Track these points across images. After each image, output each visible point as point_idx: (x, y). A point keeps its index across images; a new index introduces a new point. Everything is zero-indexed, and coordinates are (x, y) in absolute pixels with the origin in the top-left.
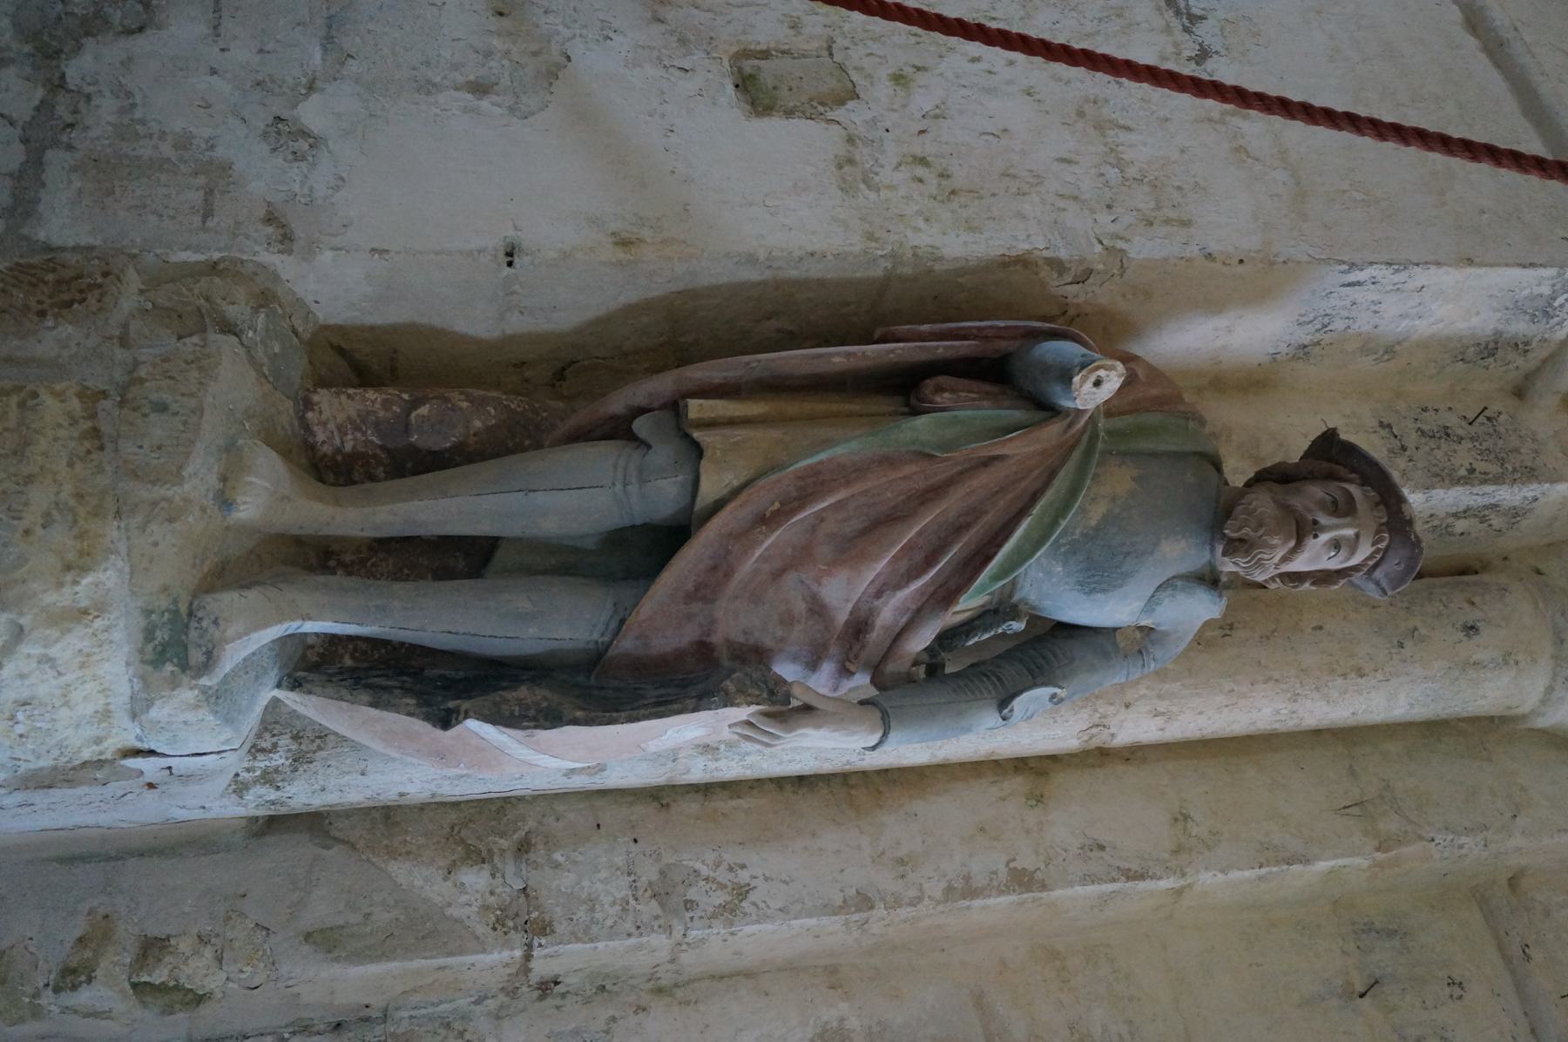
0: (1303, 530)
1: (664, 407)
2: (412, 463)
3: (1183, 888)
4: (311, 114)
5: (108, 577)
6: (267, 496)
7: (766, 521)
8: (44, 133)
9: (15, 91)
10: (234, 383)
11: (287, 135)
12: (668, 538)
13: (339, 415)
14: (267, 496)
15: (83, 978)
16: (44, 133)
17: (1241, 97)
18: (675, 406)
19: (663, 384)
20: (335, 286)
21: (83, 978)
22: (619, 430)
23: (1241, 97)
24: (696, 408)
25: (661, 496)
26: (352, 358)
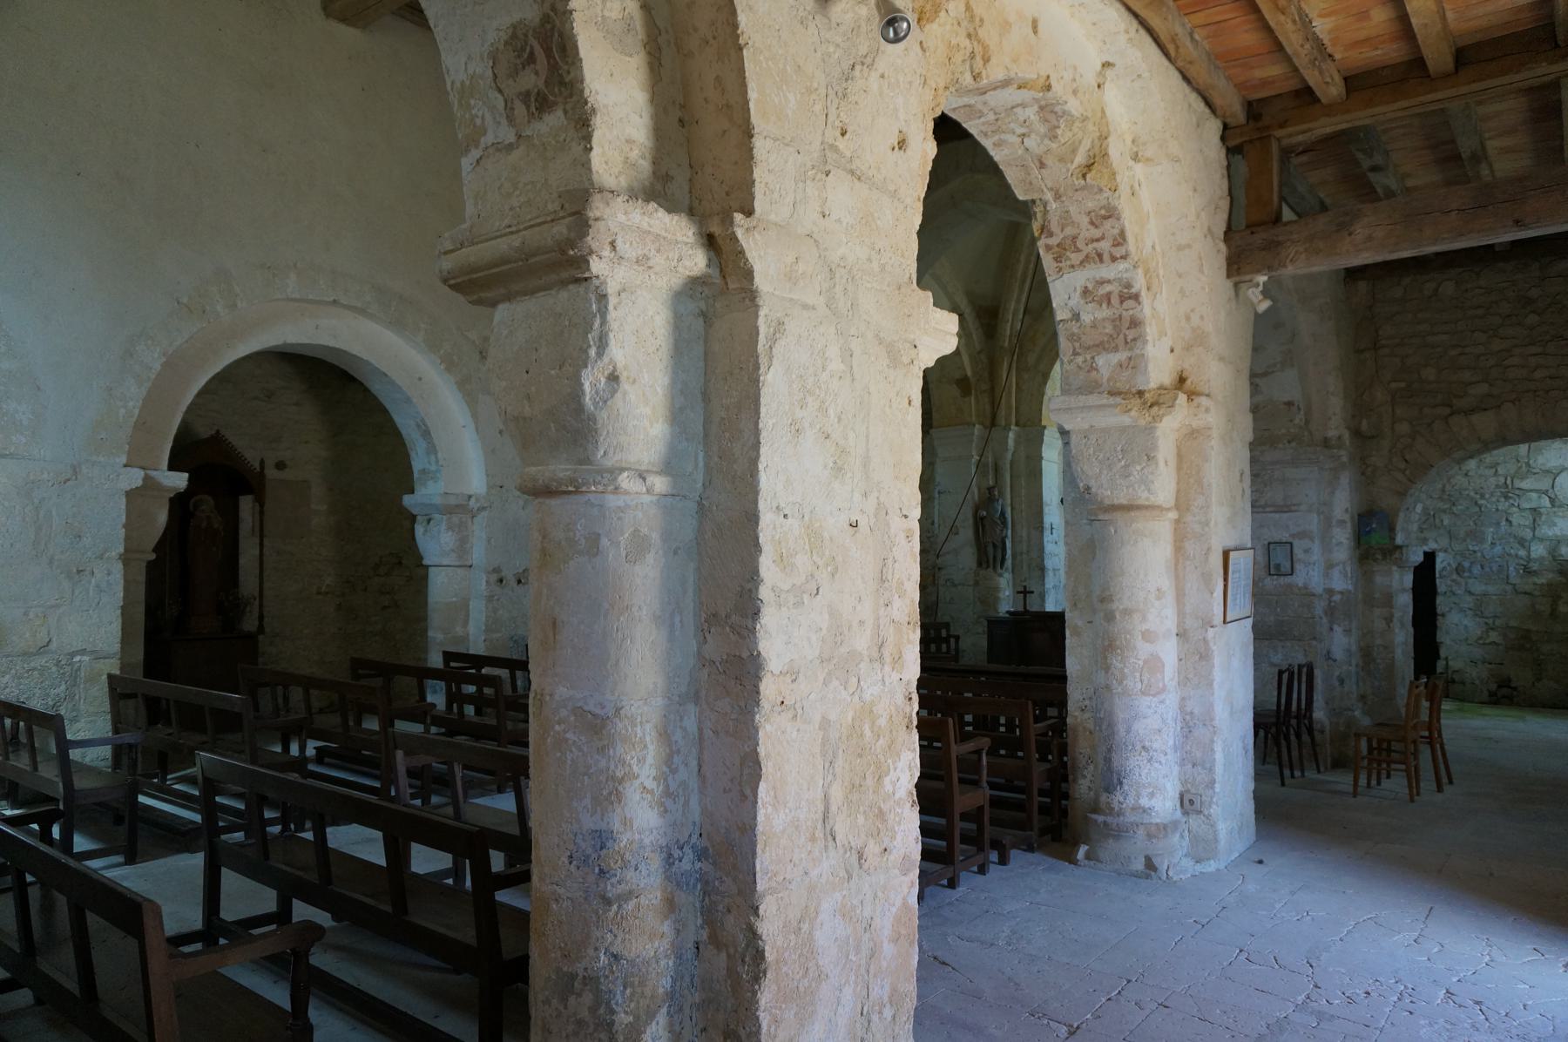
10: (982, 572)
20: (974, 565)
26: (980, 564)
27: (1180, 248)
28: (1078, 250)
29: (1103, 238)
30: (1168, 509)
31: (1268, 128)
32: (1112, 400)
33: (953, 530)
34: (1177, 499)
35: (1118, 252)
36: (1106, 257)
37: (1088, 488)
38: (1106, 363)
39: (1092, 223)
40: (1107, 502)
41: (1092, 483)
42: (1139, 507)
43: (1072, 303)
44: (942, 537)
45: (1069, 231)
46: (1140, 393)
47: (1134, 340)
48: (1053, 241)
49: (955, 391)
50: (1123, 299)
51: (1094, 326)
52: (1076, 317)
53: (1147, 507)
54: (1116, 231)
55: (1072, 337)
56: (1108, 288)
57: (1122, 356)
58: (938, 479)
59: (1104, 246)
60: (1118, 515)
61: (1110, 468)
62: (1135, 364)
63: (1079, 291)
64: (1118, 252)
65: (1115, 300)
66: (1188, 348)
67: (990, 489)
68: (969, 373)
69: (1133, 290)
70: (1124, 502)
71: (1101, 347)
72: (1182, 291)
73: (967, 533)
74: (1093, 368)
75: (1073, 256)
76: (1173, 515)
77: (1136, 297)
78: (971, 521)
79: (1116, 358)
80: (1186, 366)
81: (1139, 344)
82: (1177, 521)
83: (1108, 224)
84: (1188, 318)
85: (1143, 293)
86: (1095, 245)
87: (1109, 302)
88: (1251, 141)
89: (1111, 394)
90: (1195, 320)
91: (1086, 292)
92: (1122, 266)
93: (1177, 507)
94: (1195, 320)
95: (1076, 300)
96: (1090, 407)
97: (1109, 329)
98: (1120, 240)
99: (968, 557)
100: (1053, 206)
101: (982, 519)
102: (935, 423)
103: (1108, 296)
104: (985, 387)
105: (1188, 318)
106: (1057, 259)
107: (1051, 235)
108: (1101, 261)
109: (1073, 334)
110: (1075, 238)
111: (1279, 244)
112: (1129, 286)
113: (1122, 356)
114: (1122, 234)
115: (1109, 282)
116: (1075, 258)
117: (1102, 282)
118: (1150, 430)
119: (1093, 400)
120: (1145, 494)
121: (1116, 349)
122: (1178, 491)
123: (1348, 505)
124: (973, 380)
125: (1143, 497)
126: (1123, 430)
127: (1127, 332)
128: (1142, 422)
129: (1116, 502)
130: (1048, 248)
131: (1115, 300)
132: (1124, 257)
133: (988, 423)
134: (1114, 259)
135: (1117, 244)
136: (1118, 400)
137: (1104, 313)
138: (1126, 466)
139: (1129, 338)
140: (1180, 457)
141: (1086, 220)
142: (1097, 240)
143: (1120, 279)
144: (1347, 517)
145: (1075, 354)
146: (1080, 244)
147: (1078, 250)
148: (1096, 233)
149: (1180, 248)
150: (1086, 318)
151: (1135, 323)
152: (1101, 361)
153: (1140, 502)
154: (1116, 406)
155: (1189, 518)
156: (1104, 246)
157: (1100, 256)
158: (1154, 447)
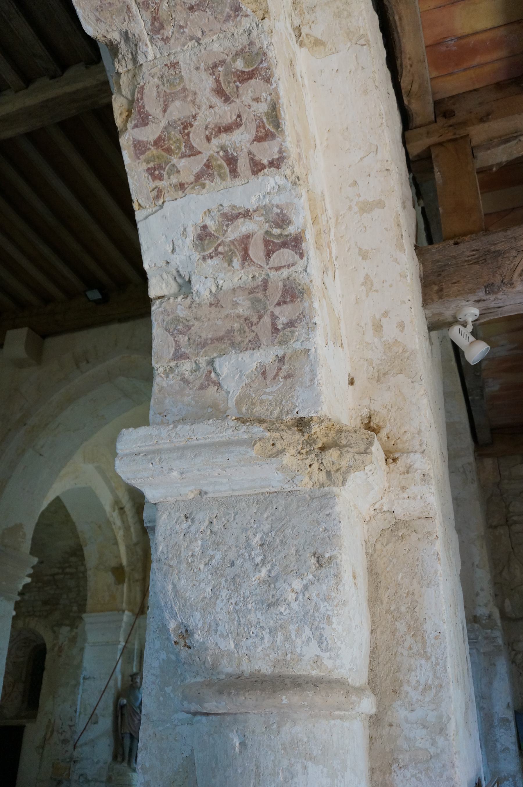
0: (137, 682)
1: (263, 167)
2: (123, 754)
3: (253, 71)
4: (96, 760)
5: (130, 774)
6: (125, 764)
7: (131, 728)
8: (96, 781)
9: (92, 783)
10: (117, 766)
11: (97, 763)
12: (131, 734)
13: (119, 759)
14: (125, 764)
15: (238, 73)
16: (96, 781)
17: (100, 699)
18: (122, 734)
19: (120, 735)
20: (110, 759)
21: (238, 73)
22: (123, 738)
23: (100, 699)
24: (122, 732)
25: (128, 736)
26: (115, 757)
27: (366, 207)
28: (194, 152)
29: (238, 124)
30: (359, 690)
31: (464, 124)
32: (243, 432)
33: (93, 719)
34: (372, 670)
35: (266, 152)
36: (243, 164)
37: (186, 633)
38: (235, 369)
39: (219, 92)
40: (228, 668)
41: (195, 620)
42: (298, 683)
43: (177, 260)
44: (80, 727)
45: (178, 110)
46: (302, 424)
47: (291, 324)
48: (149, 134)
49: (110, 578)
50: (271, 248)
51: (216, 304)
52: (185, 286)
53: (315, 684)
54: (263, 108)
55: (176, 327)
56: (245, 227)
57: (266, 355)
58: (85, 664)
59: (241, 139)
60: (248, 700)
61: (235, 583)
62: (288, 370)
63: (192, 233)
64: (266, 152)
65: (257, 251)
66: (380, 377)
67: (133, 677)
68: (124, 562)
69: (291, 230)
70: (264, 667)
71: (228, 341)
72: (367, 282)
73: (106, 723)
74: (211, 379)
75: (182, 164)
76: (367, 705)
77: (295, 243)
78: (111, 709)
79: (252, 360)
80: (376, 407)
81: (300, 330)
82: (375, 721)
83: (249, 90)
84: (378, 327)
85: (309, 235)
86: (224, 139)
87: (246, 255)
88: (441, 144)
89: (242, 420)
90: (390, 331)
91: (204, 236)
92: (271, 180)
93: (373, 685)
94: (390, 331)
95: (186, 254)
96: (197, 449)
97: (243, 308)
98: (270, 127)
99: (104, 750)
100: (149, 52)
101: (122, 707)
102: (89, 607)
103: (245, 242)
104: (137, 576)
105: (378, 327)
106: (156, 173)
107: (144, 120)
108: (234, 173)
109: (177, 320)
110: (187, 125)
111: (499, 254)
112: (282, 221)
113: (266, 355)
114: (274, 114)
115: (247, 214)
116: (187, 167)
117: (231, 217)
118: (321, 500)
119: (206, 431)
120: (312, 650)
121: (255, 344)
122: (374, 650)
123: (509, 700)
124: (127, 569)
125: (306, 656)
126: (266, 499)
127: (278, 310)
128: (305, 484)
129: (246, 668)
130: (140, 148)
131: (257, 251)
132: (275, 164)
133: (137, 610)
134: (257, 168)
135: (264, 136)
136: (258, 430)
137: (237, 276)
138: (271, 581)
139: (282, 320)
140: (373, 573)
141: (209, 83)
142: (228, 129)
143: (266, 209)
144: (510, 715)
145: (179, 356)
146: (197, 140)
147: (194, 152)
148: (226, 113)
149: (366, 207)
150: (203, 288)
151: (292, 293)
152: (225, 366)
153: (304, 669)
154: (252, 443)
155: (400, 713)
156: (241, 139)
157: (232, 161)
158: (332, 538)
